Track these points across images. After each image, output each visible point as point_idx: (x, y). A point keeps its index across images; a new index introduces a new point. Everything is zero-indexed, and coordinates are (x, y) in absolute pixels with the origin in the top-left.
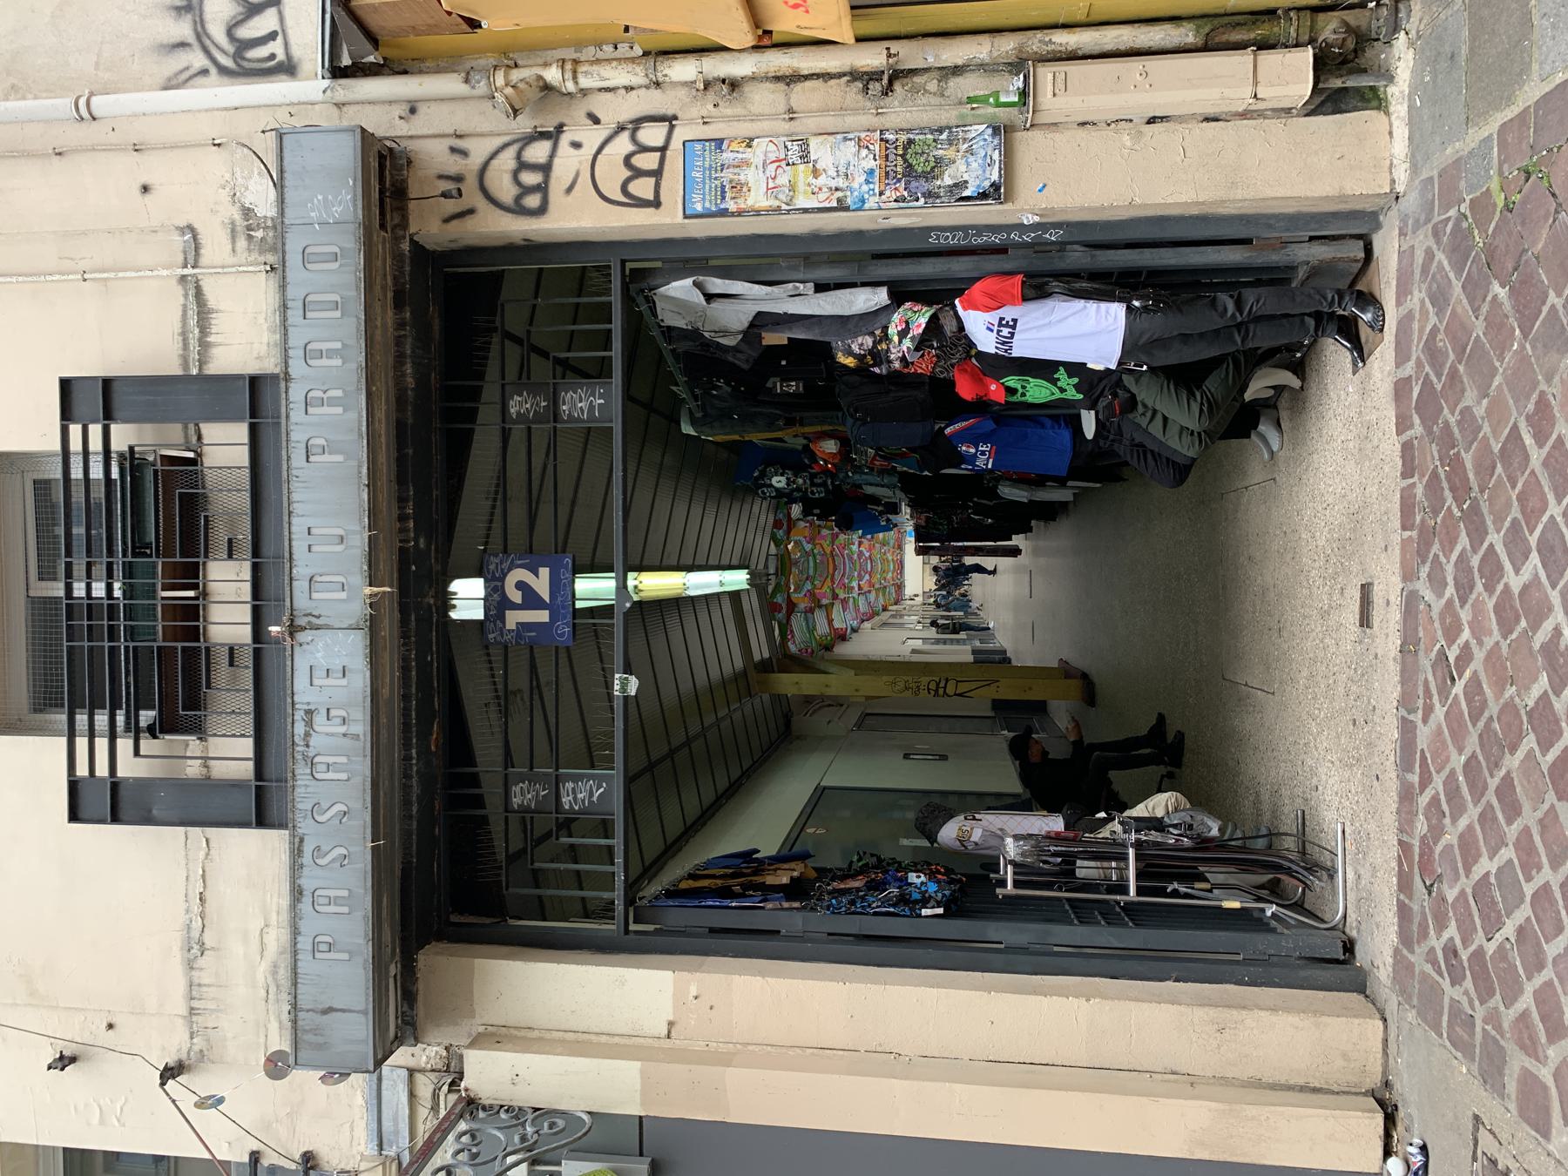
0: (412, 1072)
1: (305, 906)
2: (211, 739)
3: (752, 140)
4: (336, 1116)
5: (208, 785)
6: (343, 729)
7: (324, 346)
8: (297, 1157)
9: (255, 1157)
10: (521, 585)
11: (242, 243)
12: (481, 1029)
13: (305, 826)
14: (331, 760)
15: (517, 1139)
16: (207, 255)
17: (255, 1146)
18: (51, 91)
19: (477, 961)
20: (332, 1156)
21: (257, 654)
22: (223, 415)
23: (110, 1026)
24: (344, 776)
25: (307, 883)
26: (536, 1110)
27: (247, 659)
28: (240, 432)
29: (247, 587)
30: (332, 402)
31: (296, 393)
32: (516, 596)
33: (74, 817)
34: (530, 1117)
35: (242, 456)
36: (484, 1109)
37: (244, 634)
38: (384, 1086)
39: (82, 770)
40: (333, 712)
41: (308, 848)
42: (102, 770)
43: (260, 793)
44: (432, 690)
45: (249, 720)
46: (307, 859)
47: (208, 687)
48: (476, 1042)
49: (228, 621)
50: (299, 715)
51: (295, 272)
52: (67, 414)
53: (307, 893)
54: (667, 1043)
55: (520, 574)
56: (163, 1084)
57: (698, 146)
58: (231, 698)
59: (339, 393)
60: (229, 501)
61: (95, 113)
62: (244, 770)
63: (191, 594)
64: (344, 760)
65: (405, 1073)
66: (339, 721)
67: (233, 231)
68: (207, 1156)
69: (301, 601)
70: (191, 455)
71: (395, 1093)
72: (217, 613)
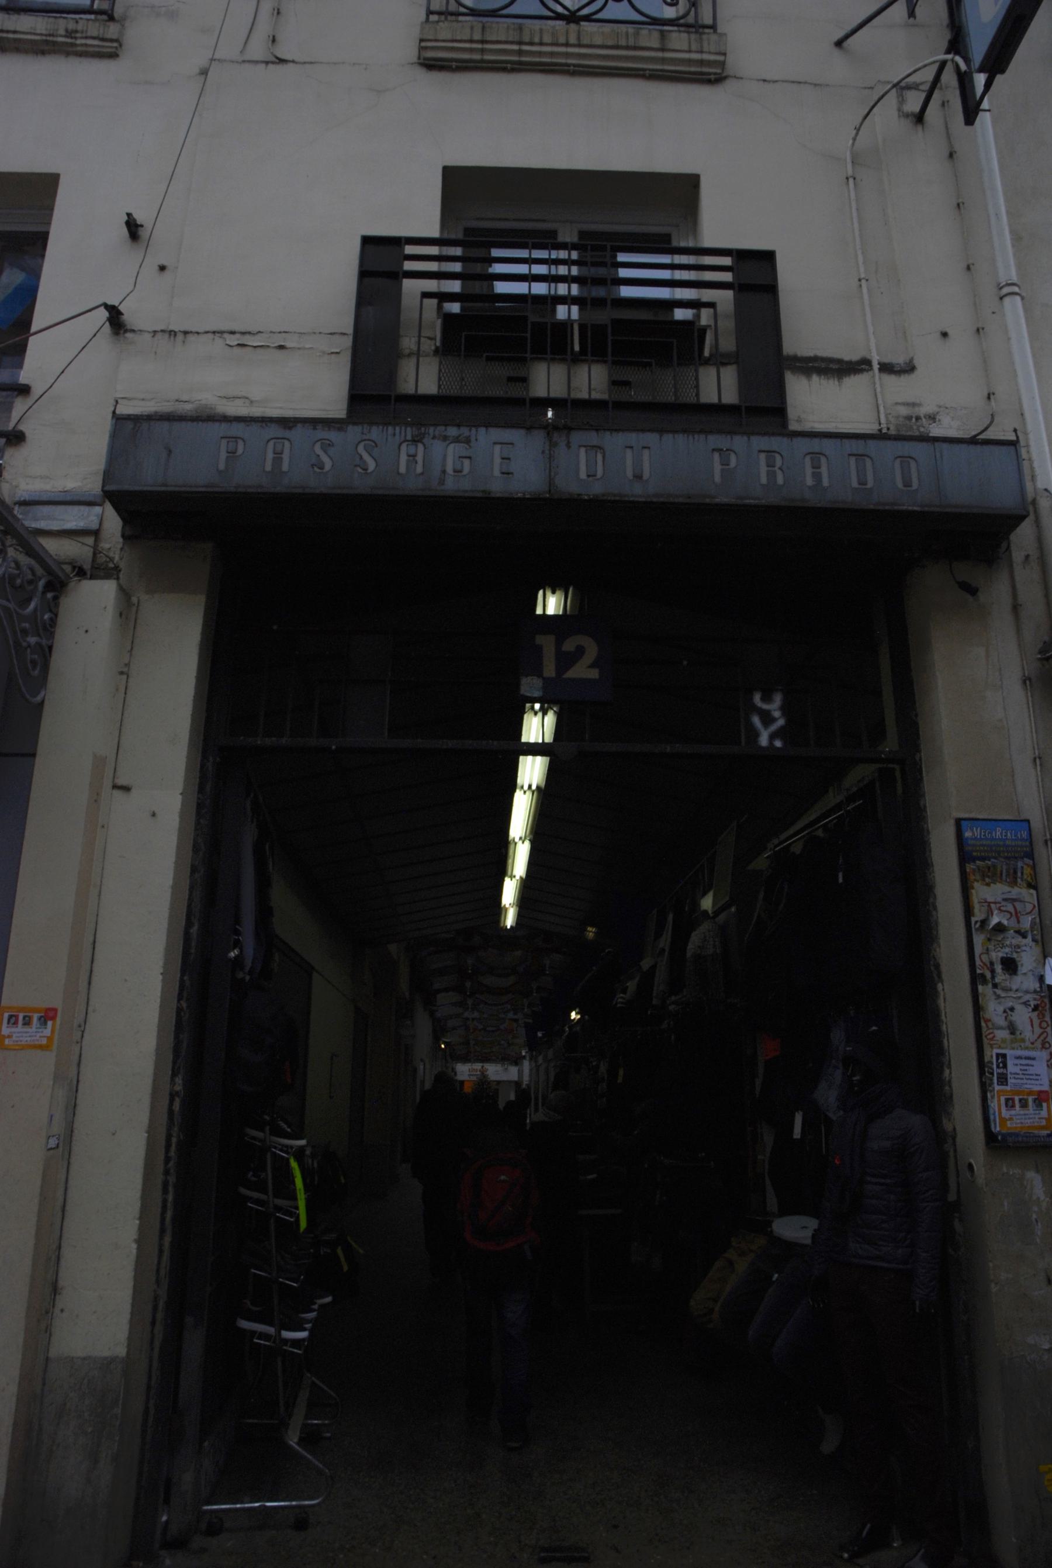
0: (96, 533)
1: (274, 431)
2: (438, 359)
3: (1035, 888)
4: (61, 459)
5: (393, 355)
6: (449, 469)
7: (824, 470)
8: (22, 427)
9: (24, 390)
10: (580, 651)
11: (904, 411)
12: (134, 600)
13: (354, 432)
14: (420, 458)
15: (27, 625)
16: (890, 380)
17: (37, 390)
18: (1019, 266)
19: (201, 600)
20: (14, 458)
21: (519, 402)
22: (744, 383)
23: (162, 268)
24: (403, 469)
25: (298, 433)
26: (50, 648)
27: (515, 391)
28: (730, 397)
29: (584, 395)
30: (771, 475)
31: (776, 443)
32: (569, 646)
33: (367, 241)
34: (44, 642)
35: (709, 395)
36: (56, 598)
37: (539, 390)
38: (82, 508)
39: (409, 250)
40: (467, 462)
41: (333, 436)
42: (409, 266)
43: (383, 399)
44: (503, 543)
45: (454, 391)
46: (321, 433)
47: (488, 359)
48: (125, 593)
49: (547, 379)
50: (465, 431)
51: (891, 449)
52: (742, 256)
53: (287, 434)
54: (108, 783)
55: (592, 651)
56: (107, 306)
57: (1025, 835)
58: (479, 377)
59: (780, 480)
60: (663, 384)
61: (1007, 300)
62: (407, 386)
63: (577, 348)
64: (419, 469)
65: (94, 526)
66: (459, 467)
67: (914, 405)
68: (33, 329)
69: (577, 437)
70: (707, 353)
71: (73, 518)
72: (559, 371)
